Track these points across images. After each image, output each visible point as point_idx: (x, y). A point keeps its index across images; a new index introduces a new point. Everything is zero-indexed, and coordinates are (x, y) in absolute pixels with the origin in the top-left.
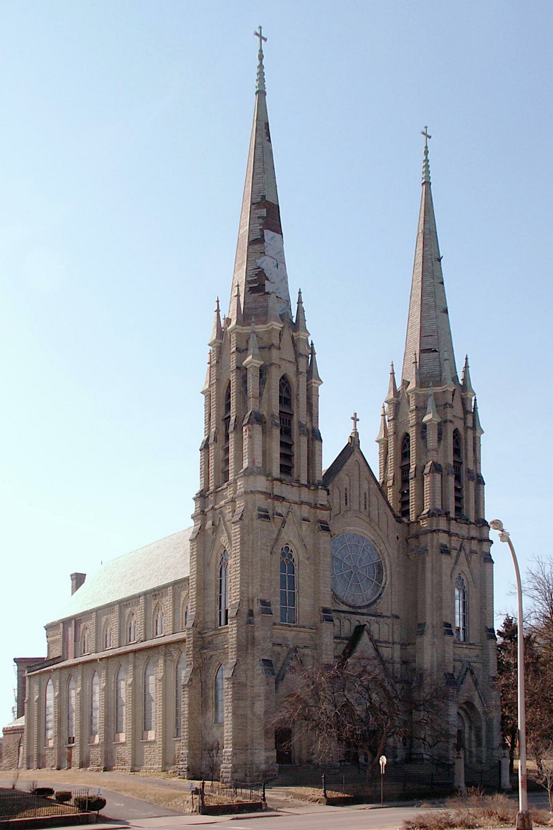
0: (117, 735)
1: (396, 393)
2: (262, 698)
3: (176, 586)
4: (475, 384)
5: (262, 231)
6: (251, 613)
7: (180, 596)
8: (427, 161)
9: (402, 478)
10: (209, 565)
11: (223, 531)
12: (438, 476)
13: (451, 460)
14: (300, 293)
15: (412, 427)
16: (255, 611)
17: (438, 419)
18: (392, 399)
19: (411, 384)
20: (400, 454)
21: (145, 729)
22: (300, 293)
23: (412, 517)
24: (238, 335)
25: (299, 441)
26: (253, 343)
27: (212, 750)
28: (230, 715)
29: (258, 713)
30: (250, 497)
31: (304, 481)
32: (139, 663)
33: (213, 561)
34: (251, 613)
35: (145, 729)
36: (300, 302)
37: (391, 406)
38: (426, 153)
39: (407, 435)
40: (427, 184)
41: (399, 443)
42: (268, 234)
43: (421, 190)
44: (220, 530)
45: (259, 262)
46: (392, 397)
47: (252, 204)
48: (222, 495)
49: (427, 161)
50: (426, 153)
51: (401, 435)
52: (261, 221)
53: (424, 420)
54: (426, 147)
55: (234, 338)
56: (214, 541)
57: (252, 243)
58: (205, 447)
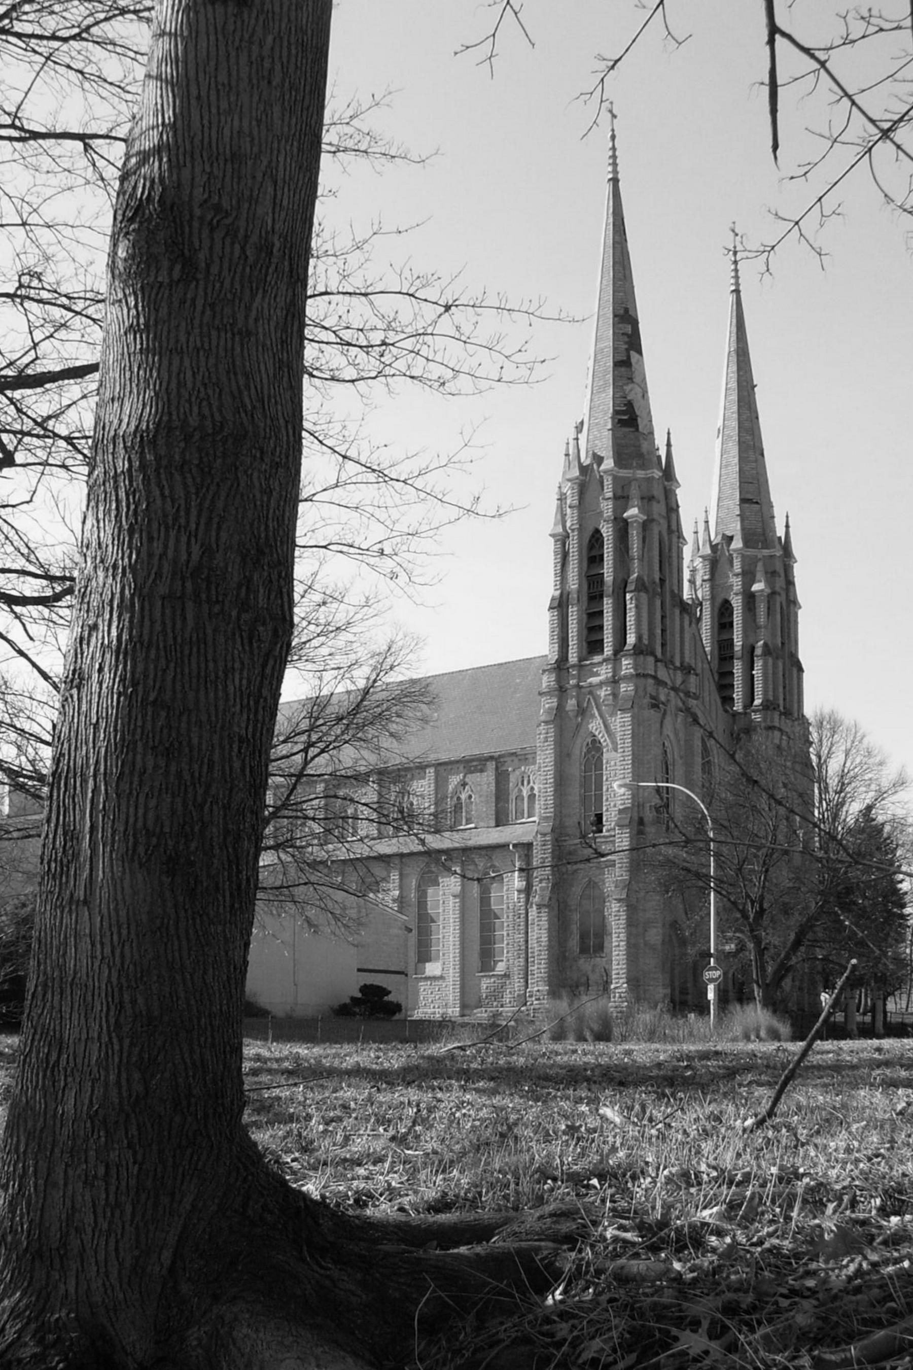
0: (420, 965)
2: (660, 925)
3: (441, 768)
5: (628, 350)
6: (641, 822)
7: (446, 781)
8: (614, 149)
9: (720, 655)
10: (569, 755)
11: (593, 716)
14: (669, 434)
15: (736, 594)
16: (646, 819)
17: (768, 591)
20: (716, 624)
21: (419, 961)
22: (669, 434)
23: (738, 707)
24: (615, 479)
25: (673, 614)
26: (634, 492)
27: (577, 987)
28: (622, 943)
30: (642, 680)
31: (678, 664)
32: (407, 870)
33: (577, 752)
34: (641, 822)
35: (419, 961)
36: (669, 445)
37: (707, 563)
38: (613, 137)
42: (633, 353)
45: (627, 388)
47: (615, 316)
48: (591, 671)
49: (614, 149)
50: (613, 137)
51: (719, 600)
52: (626, 339)
54: (613, 130)
55: (608, 482)
56: (579, 726)
57: (617, 364)
58: (560, 605)
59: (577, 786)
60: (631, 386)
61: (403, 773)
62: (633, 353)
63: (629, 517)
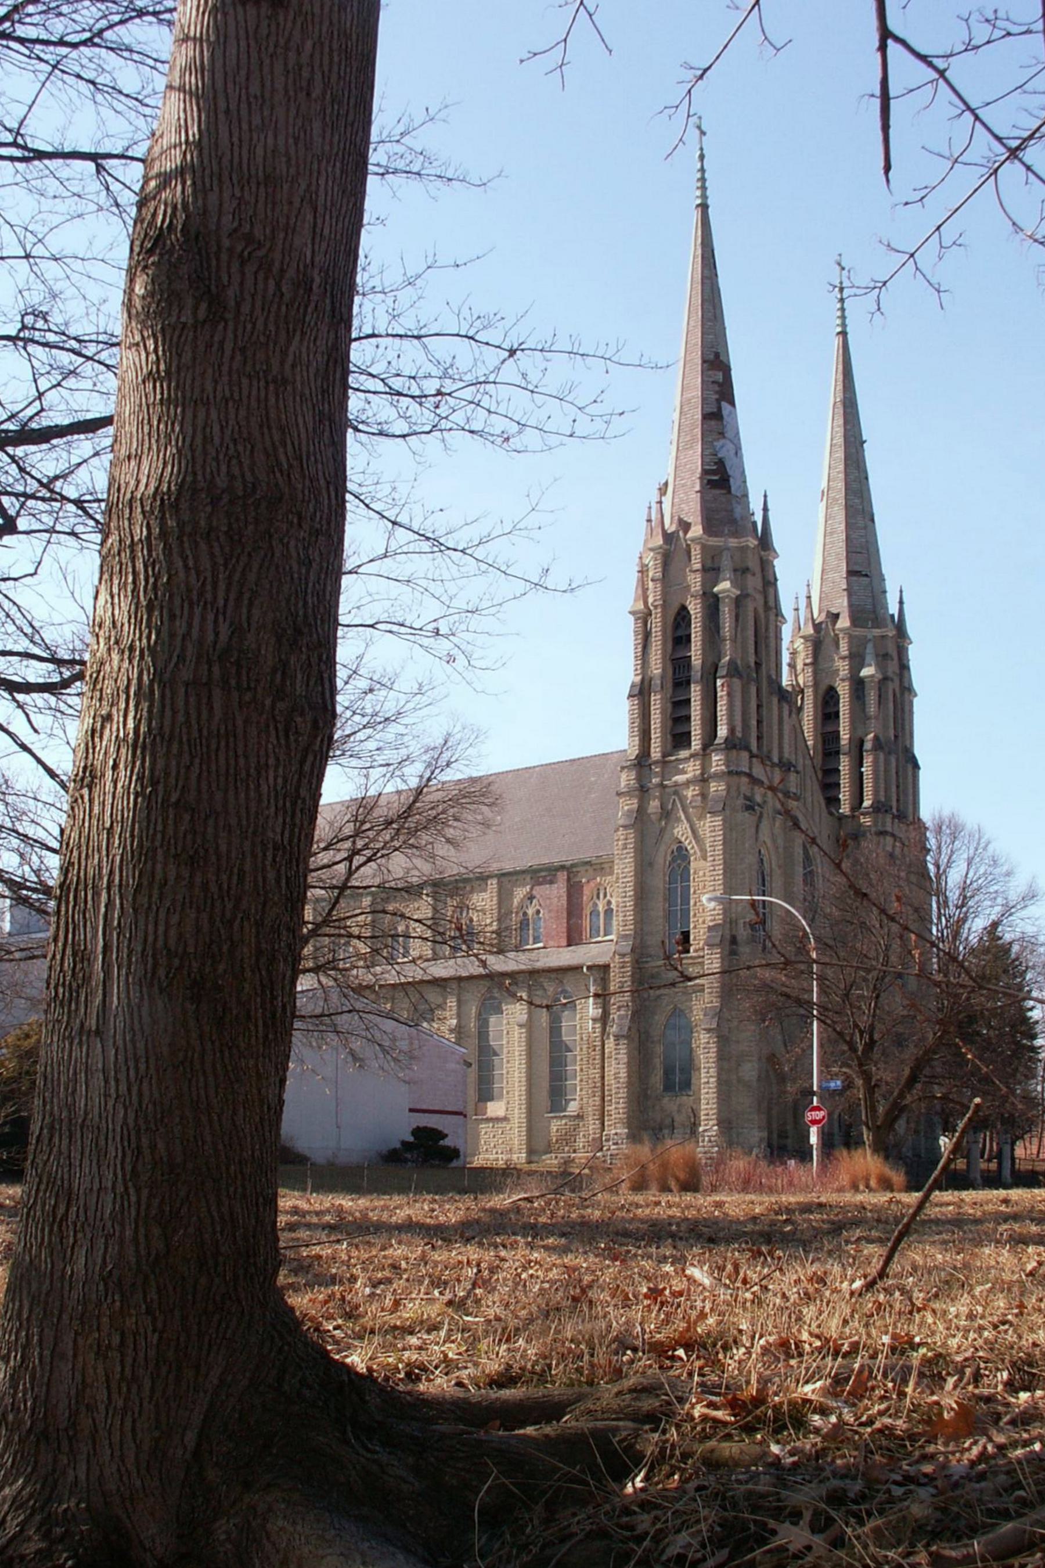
1: (668, 537)
4: (778, 540)
5: (718, 401)
6: (734, 940)
7: (511, 894)
8: (702, 170)
10: (651, 864)
11: (679, 820)
12: (736, 681)
13: (752, 659)
14: (765, 496)
16: (739, 938)
18: (660, 547)
19: (693, 528)
21: (480, 1100)
22: (765, 496)
24: (704, 548)
25: (770, 702)
26: (726, 563)
27: (661, 1129)
28: (712, 1080)
29: (747, 1078)
30: (735, 778)
32: (467, 996)
33: (661, 861)
34: (734, 940)
35: (480, 1100)
36: (765, 509)
38: (702, 157)
39: (684, 608)
40: (704, 207)
41: (671, 619)
42: (724, 404)
43: (695, 216)
44: (673, 816)
45: (718, 444)
46: (661, 542)
47: (704, 361)
48: (676, 767)
49: (702, 170)
50: (702, 157)
52: (717, 388)
53: (716, 589)
54: (701, 149)
55: (696, 552)
56: (662, 831)
57: (706, 417)
58: (641, 692)
59: (661, 899)
60: (722, 442)
61: (461, 885)
62: (724, 404)
63: (720, 592)
